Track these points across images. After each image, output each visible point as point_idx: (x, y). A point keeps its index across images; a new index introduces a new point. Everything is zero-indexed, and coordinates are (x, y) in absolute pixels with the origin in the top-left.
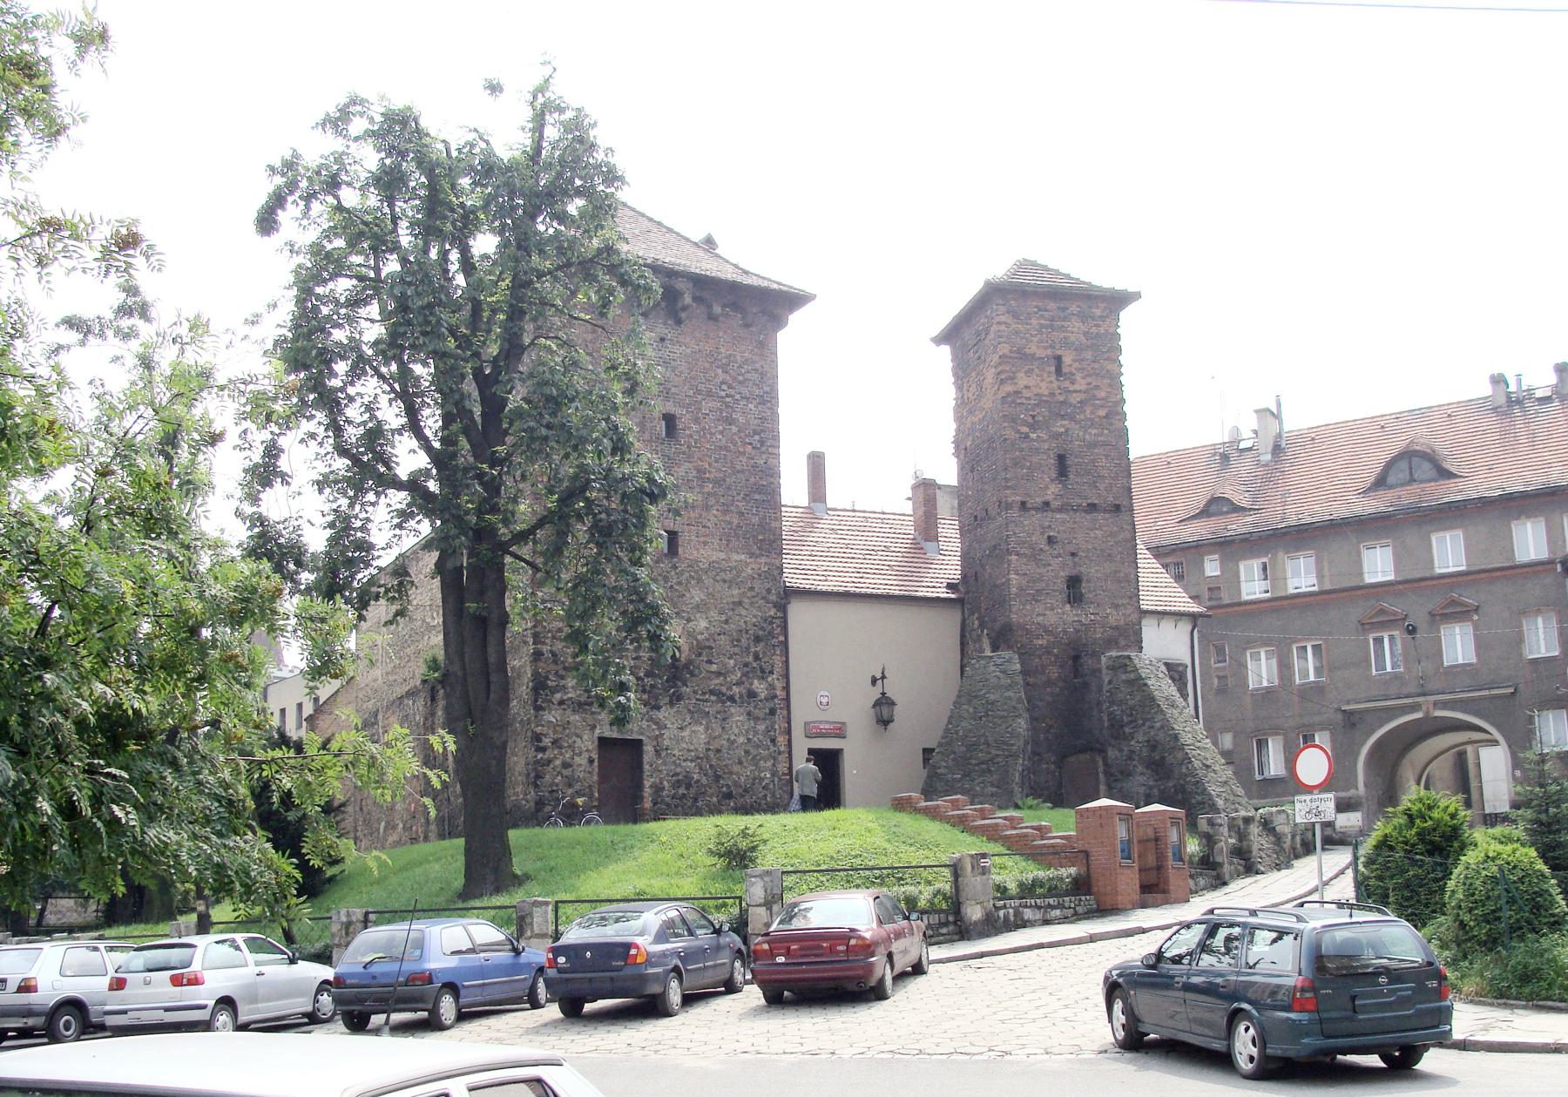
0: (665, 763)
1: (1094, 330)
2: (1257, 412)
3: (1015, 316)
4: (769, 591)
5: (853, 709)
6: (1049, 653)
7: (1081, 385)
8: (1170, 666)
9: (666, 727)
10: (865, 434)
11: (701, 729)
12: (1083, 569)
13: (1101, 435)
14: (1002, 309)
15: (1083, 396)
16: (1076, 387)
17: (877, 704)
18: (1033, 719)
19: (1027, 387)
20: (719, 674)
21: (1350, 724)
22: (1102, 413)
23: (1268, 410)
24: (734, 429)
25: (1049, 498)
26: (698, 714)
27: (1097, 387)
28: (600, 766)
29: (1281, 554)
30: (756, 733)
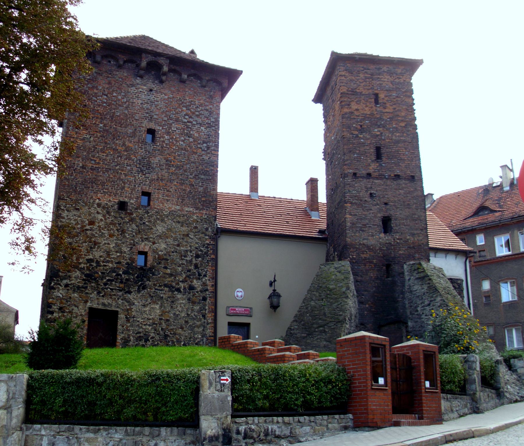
0: (132, 326)
1: (397, 80)
2: (501, 167)
3: (351, 72)
4: (207, 229)
5: (259, 302)
6: (371, 262)
7: (389, 109)
8: (452, 281)
9: (134, 304)
11: (157, 307)
12: (392, 212)
13: (402, 136)
14: (342, 68)
15: (391, 116)
16: (387, 110)
17: (270, 297)
18: (360, 303)
19: (357, 110)
20: (171, 275)
22: (403, 124)
23: (506, 166)
24: (191, 140)
25: (371, 171)
26: (155, 298)
27: (399, 110)
28: (89, 325)
29: (516, 231)
30: (193, 310)
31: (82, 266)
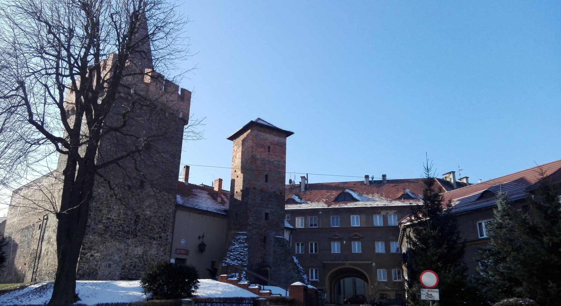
10: (209, 160)
21: (324, 267)
31: (104, 221)
